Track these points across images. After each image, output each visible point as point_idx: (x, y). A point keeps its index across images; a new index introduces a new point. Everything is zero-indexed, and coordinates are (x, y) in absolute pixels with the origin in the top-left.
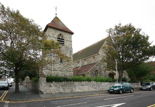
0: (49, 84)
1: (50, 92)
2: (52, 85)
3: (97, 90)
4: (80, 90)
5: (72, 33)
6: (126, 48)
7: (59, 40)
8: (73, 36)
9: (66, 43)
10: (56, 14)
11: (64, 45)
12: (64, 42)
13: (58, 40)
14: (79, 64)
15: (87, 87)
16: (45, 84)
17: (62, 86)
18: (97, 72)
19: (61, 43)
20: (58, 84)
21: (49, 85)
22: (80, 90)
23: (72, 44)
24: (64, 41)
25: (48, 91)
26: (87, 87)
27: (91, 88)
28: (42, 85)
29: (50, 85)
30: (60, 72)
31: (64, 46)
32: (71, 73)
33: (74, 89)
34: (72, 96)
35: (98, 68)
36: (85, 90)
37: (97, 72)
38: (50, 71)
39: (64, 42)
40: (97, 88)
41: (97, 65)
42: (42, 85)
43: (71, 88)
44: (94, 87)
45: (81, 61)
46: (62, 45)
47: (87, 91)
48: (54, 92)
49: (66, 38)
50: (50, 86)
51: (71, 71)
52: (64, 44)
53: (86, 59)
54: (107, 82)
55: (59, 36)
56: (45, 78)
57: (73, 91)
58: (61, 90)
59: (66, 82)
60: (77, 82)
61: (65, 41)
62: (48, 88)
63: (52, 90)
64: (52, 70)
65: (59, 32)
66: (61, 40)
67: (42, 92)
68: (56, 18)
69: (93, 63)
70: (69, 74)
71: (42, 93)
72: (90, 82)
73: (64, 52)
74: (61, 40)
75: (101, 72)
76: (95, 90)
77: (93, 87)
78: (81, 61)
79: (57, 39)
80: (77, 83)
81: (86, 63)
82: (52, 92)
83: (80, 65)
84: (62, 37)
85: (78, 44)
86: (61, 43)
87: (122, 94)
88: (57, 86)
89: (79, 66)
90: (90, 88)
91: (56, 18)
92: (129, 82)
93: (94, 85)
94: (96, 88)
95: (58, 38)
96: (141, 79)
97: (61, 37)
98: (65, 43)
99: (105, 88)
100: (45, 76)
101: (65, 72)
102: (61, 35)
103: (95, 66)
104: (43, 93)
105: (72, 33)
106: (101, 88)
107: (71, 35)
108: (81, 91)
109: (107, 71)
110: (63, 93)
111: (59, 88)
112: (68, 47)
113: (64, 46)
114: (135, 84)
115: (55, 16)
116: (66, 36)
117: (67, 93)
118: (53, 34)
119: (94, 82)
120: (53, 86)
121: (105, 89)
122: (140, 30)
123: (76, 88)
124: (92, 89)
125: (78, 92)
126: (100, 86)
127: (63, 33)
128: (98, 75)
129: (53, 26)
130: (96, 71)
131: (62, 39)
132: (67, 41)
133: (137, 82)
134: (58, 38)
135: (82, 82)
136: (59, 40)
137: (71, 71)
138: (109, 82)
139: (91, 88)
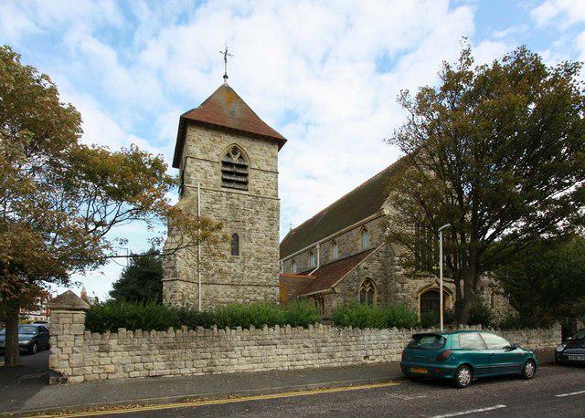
0: (98, 342)
1: (104, 376)
2: (113, 343)
3: (335, 365)
4: (250, 366)
5: (279, 142)
6: (496, 135)
7: (228, 169)
8: (284, 154)
9: (256, 181)
10: (225, 77)
11: (249, 186)
12: (246, 175)
13: (224, 172)
14: (313, 260)
15: (285, 352)
16: (80, 341)
17: (161, 348)
18: (371, 286)
19: (238, 182)
20: (141, 339)
21: (100, 345)
22: (250, 366)
23: (277, 183)
24: (245, 172)
25: (92, 372)
26: (285, 352)
27: (307, 356)
28: (61, 344)
29: (104, 342)
30: (230, 290)
31: (247, 190)
32: (269, 290)
33: (220, 361)
34: (181, 401)
35: (375, 272)
36: (274, 365)
37: (371, 286)
38: (191, 285)
39: (249, 177)
40: (339, 354)
41: (371, 260)
42: (61, 344)
43: (209, 355)
44: (323, 349)
45: (318, 247)
46: (241, 187)
47: (286, 368)
48: (121, 375)
49: (256, 160)
50: (104, 349)
51: (270, 286)
52: (246, 183)
53: (337, 240)
54: (390, 325)
55: (228, 155)
56: (81, 316)
57: (218, 370)
58: (159, 367)
59: (183, 332)
60: (239, 328)
61: (251, 173)
62: (92, 357)
63: (112, 368)
64: (200, 282)
65: (227, 142)
66: (234, 169)
67: (60, 374)
68: (226, 90)
69: (360, 251)
70: (265, 296)
71: (61, 379)
72: (306, 327)
73: (246, 213)
74: (234, 169)
75: (386, 283)
76: (325, 362)
77: (319, 352)
78: (318, 247)
79: (220, 167)
80: (236, 335)
81: (335, 254)
82: (111, 377)
83: (315, 262)
84: (241, 157)
85: (308, 183)
86: (238, 182)
87: (468, 390)
88: (139, 348)
89: (313, 265)
90: (303, 357)
91: (226, 90)
92: (504, 327)
93: (324, 341)
94: (331, 357)
95: (225, 164)
96: (569, 310)
97: (235, 160)
98: (252, 181)
99: (376, 352)
100: (76, 307)
101: (250, 288)
102: (235, 150)
103: (363, 264)
104: (65, 381)
105: (279, 142)
106: (360, 354)
107: (274, 149)
108: (259, 368)
109: (411, 282)
110: (169, 381)
111: (145, 359)
112: (262, 193)
113: (245, 193)
114: (533, 332)
115: (221, 82)
116: (256, 153)
117: (184, 380)
118: (204, 151)
119: (324, 331)
120: (119, 348)
121: (377, 360)
122: (571, 70)
123: (231, 354)
124: (309, 360)
125: (237, 377)
126: (353, 348)
127: (244, 143)
128: (376, 296)
129: (204, 120)
130: (368, 280)
131: (239, 166)
132: (258, 172)
133: (545, 325)
134: (225, 164)
135: (266, 327)
136: (241, 171)
137: (270, 286)
138: (399, 327)
139: (307, 356)
